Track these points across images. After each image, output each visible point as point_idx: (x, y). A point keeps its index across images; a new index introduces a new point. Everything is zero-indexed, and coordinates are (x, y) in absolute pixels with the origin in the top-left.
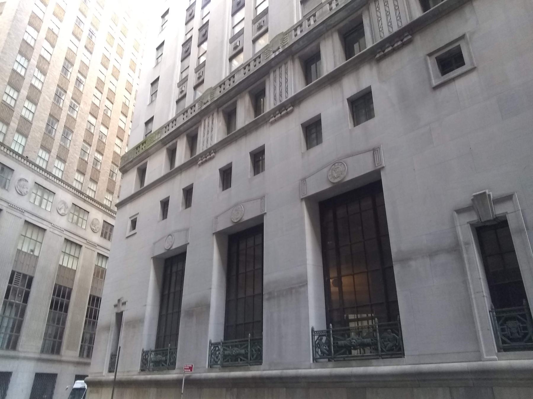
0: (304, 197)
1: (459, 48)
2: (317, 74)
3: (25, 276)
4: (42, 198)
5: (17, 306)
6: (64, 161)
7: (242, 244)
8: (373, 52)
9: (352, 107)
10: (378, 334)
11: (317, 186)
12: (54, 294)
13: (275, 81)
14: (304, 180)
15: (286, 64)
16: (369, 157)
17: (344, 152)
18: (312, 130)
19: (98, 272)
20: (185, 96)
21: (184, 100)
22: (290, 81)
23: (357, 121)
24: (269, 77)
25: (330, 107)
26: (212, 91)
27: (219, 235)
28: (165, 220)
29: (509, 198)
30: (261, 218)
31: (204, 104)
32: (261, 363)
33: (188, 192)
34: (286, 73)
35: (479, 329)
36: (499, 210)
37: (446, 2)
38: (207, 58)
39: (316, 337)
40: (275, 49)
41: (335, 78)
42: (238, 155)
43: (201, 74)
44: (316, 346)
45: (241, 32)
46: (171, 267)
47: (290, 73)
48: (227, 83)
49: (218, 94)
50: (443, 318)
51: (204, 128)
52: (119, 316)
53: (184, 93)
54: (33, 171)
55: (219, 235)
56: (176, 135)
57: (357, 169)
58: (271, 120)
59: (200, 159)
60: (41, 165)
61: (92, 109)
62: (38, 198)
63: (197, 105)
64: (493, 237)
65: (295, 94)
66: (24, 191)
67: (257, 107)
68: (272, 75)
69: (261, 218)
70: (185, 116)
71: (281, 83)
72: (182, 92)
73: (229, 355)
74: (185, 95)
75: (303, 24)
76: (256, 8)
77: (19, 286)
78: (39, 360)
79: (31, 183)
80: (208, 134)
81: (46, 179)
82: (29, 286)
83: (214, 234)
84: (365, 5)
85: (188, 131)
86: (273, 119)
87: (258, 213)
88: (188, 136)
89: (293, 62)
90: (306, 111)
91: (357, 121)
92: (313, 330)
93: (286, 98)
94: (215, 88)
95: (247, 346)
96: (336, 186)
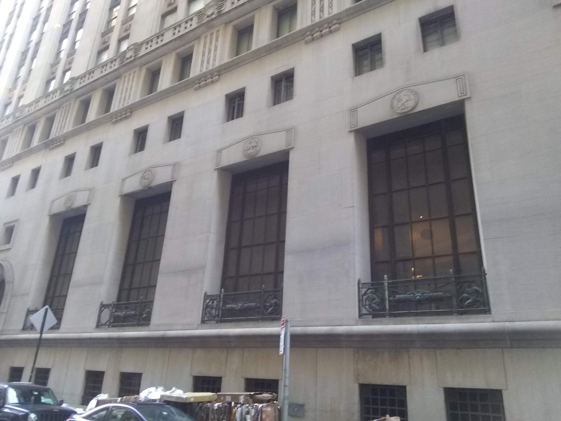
2: (249, 48)
7: (147, 210)
8: (311, 29)
9: (139, 137)
10: (387, 297)
11: (234, 157)
14: (220, 151)
16: (283, 135)
18: (235, 104)
23: (358, 70)
24: (199, 43)
26: (137, 47)
27: (224, 171)
28: (139, 154)
30: (285, 154)
31: (208, 17)
32: (148, 324)
33: (96, 151)
34: (217, 40)
37: (364, 2)
38: (137, 11)
39: (208, 301)
42: (156, 120)
43: (107, 40)
44: (206, 307)
46: (68, 226)
53: (174, 6)
55: (224, 171)
56: (91, 88)
57: (271, 145)
65: (339, 11)
69: (285, 154)
72: (105, 43)
80: (126, 91)
84: (196, 39)
85: (178, 50)
86: (198, 85)
87: (169, 180)
91: (358, 70)
94: (142, 44)
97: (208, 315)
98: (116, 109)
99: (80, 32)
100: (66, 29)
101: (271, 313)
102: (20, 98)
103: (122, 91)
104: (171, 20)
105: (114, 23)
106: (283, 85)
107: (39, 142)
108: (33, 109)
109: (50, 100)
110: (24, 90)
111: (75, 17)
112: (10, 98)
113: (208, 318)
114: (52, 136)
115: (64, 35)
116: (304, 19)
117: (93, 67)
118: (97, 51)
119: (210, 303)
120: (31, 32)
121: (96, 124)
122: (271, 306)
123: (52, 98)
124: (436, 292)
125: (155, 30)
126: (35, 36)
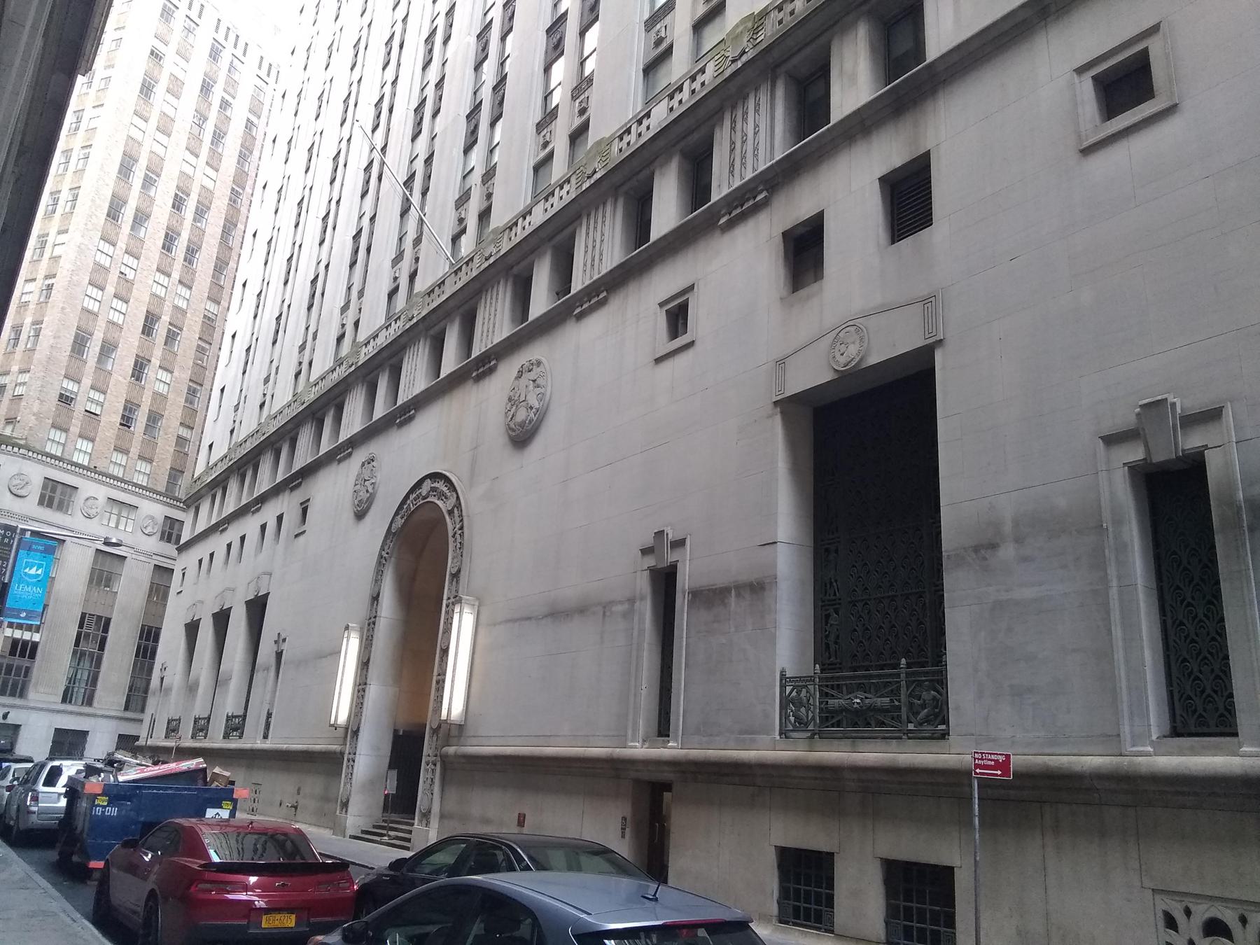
0: (779, 398)
3: (99, 618)
4: (119, 516)
5: (91, 654)
6: (150, 461)
11: (810, 374)
12: (141, 638)
13: (733, 129)
14: (781, 362)
15: (757, 89)
17: (865, 301)
18: (804, 250)
19: (149, 633)
20: (669, 51)
21: (717, 21)
25: (847, 195)
27: (790, 406)
29: (1212, 415)
31: (733, 61)
35: (1124, 687)
36: (1193, 441)
38: (598, 62)
39: (788, 689)
41: (863, 124)
49: (769, 32)
50: (1045, 665)
51: (588, 234)
52: (279, 655)
54: (103, 483)
55: (790, 406)
57: (889, 342)
58: (722, 222)
60: (115, 473)
61: (193, 373)
62: (114, 518)
63: (573, 180)
64: (1174, 496)
66: (92, 512)
67: (697, 185)
70: (548, 205)
73: (843, 710)
74: (671, 46)
77: (90, 629)
78: (121, 719)
79: (102, 500)
81: (124, 490)
82: (106, 630)
83: (776, 403)
88: (685, 155)
90: (796, 206)
92: (783, 675)
93: (754, 170)
95: (899, 688)
96: (844, 377)
97: (792, 719)
98: (580, 287)
99: (592, 36)
101: (927, 720)
103: (586, 247)
105: (556, 99)
106: (908, 201)
109: (557, 203)
110: (583, 111)
112: (395, 279)
113: (794, 726)
114: (577, 285)
115: (556, 49)
116: (943, 31)
119: (794, 694)
121: (681, 240)
122: (923, 706)
124: (1129, 688)
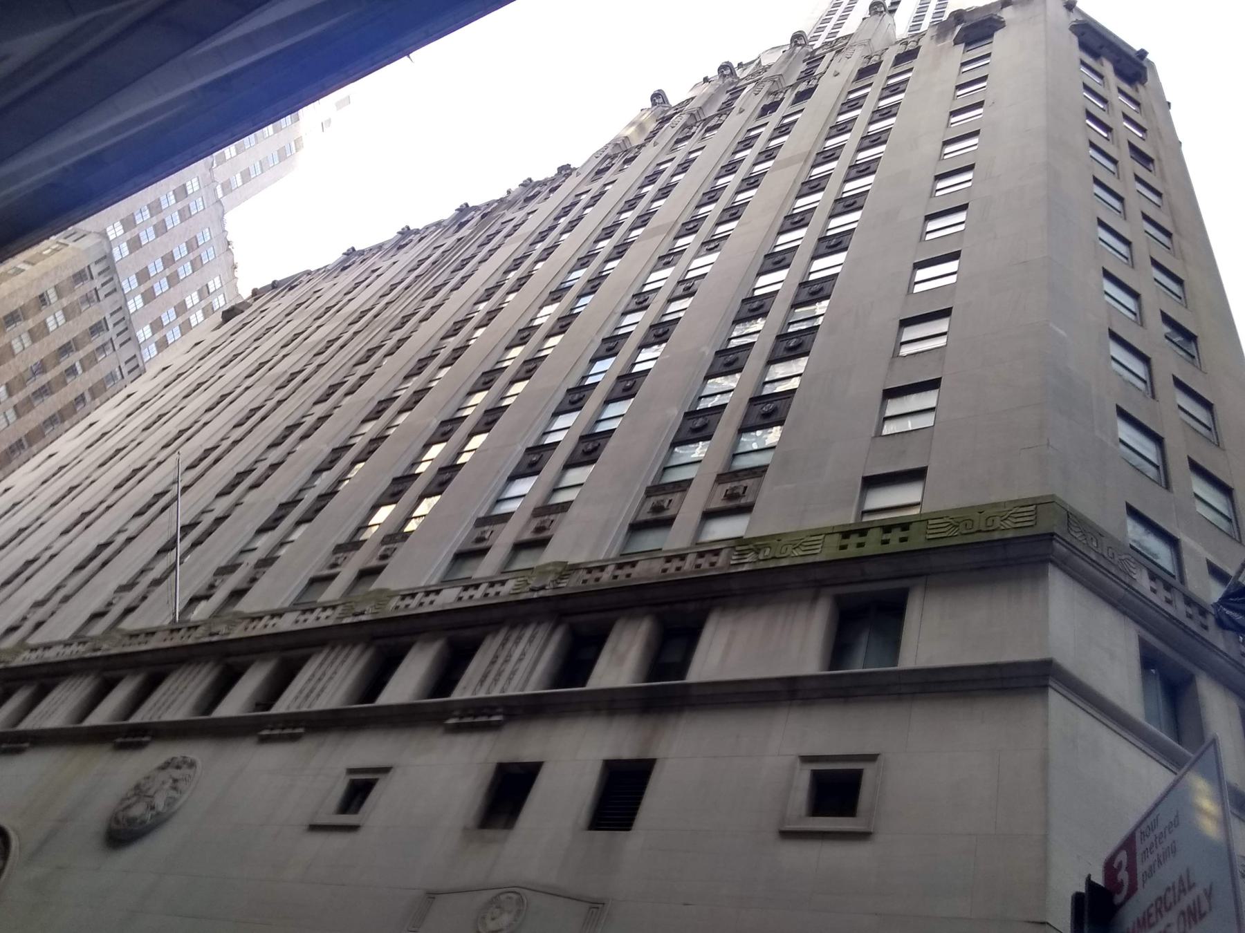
1: (859, 773)
13: (503, 645)
20: (483, 552)
22: (518, 665)
40: (358, 610)
43: (547, 525)
45: (506, 517)
47: (342, 671)
48: (875, 535)
49: (571, 584)
59: (457, 713)
68: (326, 651)
70: (302, 618)
71: (324, 674)
72: (539, 530)
75: (870, 532)
76: (665, 469)
89: (363, 652)
94: (575, 568)
98: (467, 695)
100: (281, 513)
102: (129, 611)
104: (650, 541)
107: (115, 720)
108: (258, 629)
109: (311, 621)
110: (384, 557)
111: (309, 497)
117: (286, 605)
118: (455, 550)
120: (318, 472)
121: (405, 718)
123: (266, 626)
125: (431, 577)
126: (324, 482)
